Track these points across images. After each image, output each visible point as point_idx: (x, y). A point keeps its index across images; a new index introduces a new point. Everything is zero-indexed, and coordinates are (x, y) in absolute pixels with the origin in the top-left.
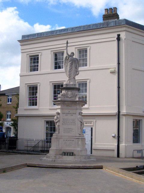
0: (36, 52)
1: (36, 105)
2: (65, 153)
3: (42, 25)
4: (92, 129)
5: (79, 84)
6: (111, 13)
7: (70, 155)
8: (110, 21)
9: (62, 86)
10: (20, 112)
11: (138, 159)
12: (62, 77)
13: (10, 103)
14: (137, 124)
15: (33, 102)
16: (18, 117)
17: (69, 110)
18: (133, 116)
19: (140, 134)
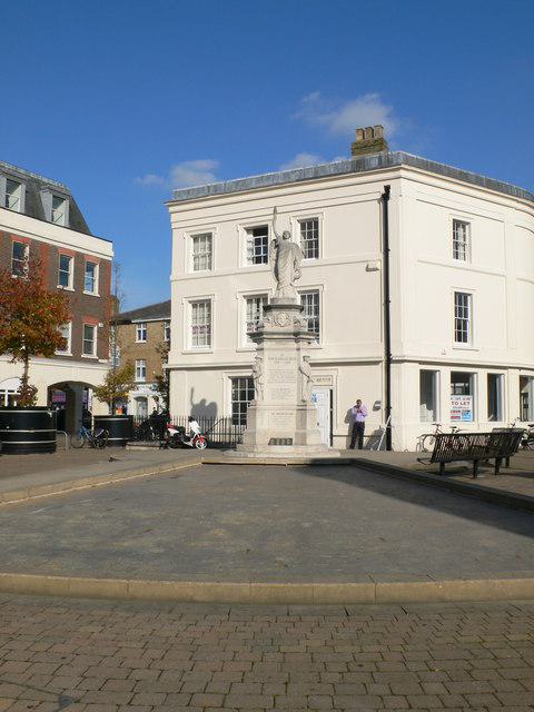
0: (205, 221)
1: (465, 341)
2: (275, 440)
3: (309, 153)
4: (331, 391)
5: (303, 298)
6: (370, 139)
7: (286, 444)
8: (368, 156)
9: (265, 299)
10: (174, 359)
11: (34, 452)
12: (262, 279)
13: (142, 341)
14: (524, 381)
15: (204, 332)
16: (168, 371)
17: (281, 352)
18: (421, 363)
19: (435, 401)
